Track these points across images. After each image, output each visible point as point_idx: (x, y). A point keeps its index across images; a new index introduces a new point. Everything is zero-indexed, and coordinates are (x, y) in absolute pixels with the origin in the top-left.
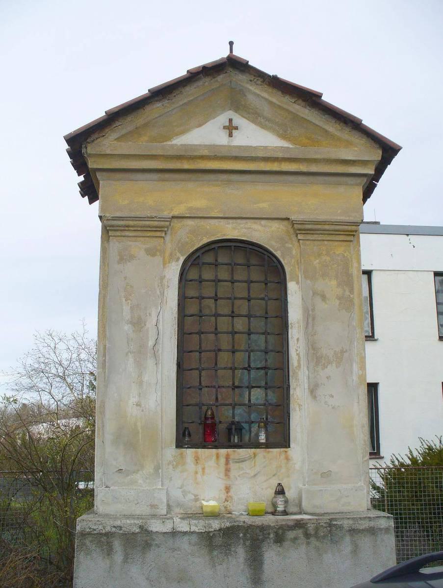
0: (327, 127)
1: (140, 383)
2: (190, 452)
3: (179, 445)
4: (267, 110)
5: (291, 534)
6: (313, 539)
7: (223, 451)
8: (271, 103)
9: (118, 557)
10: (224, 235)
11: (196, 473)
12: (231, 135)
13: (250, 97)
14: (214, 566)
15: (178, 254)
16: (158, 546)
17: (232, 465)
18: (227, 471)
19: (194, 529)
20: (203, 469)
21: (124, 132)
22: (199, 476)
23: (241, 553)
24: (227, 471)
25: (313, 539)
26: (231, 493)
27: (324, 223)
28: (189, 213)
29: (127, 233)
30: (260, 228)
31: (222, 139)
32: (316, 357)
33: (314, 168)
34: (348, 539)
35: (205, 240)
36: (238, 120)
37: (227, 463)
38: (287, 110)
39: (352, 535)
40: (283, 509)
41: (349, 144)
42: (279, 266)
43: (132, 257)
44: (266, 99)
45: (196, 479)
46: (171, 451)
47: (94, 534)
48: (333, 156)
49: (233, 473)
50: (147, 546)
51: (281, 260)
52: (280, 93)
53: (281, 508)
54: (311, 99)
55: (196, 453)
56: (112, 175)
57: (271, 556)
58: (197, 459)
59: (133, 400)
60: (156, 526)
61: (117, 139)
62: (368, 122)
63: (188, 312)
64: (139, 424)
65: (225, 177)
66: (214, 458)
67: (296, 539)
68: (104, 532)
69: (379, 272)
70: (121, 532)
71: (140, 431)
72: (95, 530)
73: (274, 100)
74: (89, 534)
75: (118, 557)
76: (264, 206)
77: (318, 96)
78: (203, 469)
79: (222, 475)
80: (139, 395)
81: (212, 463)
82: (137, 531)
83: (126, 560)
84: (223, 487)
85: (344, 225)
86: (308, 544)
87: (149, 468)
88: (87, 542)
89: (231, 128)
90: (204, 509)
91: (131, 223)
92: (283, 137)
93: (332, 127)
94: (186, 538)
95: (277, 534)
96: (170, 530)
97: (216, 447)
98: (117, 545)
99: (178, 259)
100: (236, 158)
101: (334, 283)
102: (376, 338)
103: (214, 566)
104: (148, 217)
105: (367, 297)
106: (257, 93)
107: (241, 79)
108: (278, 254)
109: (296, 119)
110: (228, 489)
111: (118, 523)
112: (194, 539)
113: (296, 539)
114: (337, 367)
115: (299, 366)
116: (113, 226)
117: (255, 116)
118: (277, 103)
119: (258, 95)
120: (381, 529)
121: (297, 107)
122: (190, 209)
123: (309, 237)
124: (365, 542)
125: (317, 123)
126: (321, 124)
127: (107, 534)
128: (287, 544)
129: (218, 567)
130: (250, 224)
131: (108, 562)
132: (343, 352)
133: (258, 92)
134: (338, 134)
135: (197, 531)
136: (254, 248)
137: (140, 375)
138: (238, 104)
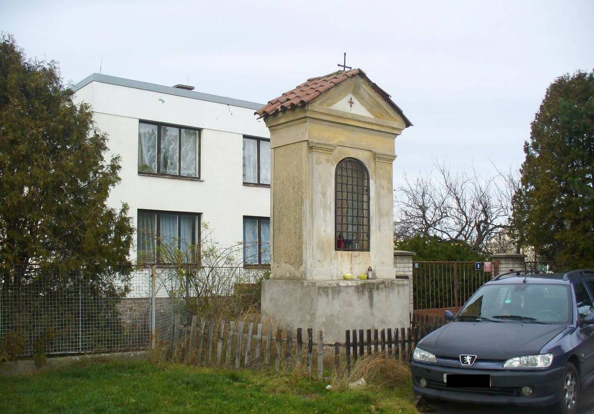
0: (390, 112)
1: (325, 221)
2: (339, 252)
4: (366, 97)
5: (381, 286)
6: (387, 288)
7: (350, 252)
8: (370, 95)
9: (330, 297)
12: (351, 106)
13: (362, 91)
14: (359, 300)
15: (335, 163)
16: (342, 292)
17: (353, 259)
18: (351, 261)
19: (353, 284)
20: (344, 260)
22: (342, 263)
23: (367, 294)
24: (351, 261)
25: (387, 288)
29: (320, 151)
30: (361, 153)
32: (381, 214)
33: (383, 129)
34: (396, 288)
36: (354, 100)
37: (351, 258)
38: (376, 100)
39: (397, 287)
40: (308, 278)
41: (395, 120)
43: (321, 163)
44: (368, 93)
46: (333, 251)
48: (390, 125)
49: (353, 262)
50: (339, 292)
53: (370, 277)
54: (385, 96)
55: (341, 253)
56: (316, 121)
57: (375, 294)
58: (342, 256)
59: (323, 229)
60: (343, 284)
61: (319, 104)
62: (404, 113)
63: (338, 190)
64: (325, 240)
65: (352, 128)
67: (382, 288)
69: (207, 130)
73: (371, 94)
74: (321, 287)
75: (330, 297)
79: (350, 263)
81: (346, 257)
83: (333, 298)
84: (350, 268)
86: (386, 290)
87: (329, 260)
88: (320, 291)
89: (351, 103)
91: (323, 146)
92: (369, 110)
93: (390, 111)
94: (351, 288)
95: (377, 286)
97: (348, 251)
98: (330, 291)
100: (359, 121)
102: (201, 179)
103: (359, 300)
106: (365, 89)
107: (361, 81)
108: (367, 166)
109: (378, 104)
110: (351, 269)
111: (330, 283)
112: (353, 288)
113: (382, 288)
114: (387, 218)
115: (373, 217)
116: (315, 147)
117: (361, 99)
118: (373, 96)
119: (366, 90)
120: (405, 284)
121: (380, 99)
122: (340, 142)
123: (380, 161)
124: (401, 289)
126: (386, 109)
127: (327, 287)
128: (380, 290)
129: (360, 300)
131: (327, 299)
132: (388, 212)
133: (366, 88)
134: (393, 115)
137: (325, 218)
138: (355, 92)
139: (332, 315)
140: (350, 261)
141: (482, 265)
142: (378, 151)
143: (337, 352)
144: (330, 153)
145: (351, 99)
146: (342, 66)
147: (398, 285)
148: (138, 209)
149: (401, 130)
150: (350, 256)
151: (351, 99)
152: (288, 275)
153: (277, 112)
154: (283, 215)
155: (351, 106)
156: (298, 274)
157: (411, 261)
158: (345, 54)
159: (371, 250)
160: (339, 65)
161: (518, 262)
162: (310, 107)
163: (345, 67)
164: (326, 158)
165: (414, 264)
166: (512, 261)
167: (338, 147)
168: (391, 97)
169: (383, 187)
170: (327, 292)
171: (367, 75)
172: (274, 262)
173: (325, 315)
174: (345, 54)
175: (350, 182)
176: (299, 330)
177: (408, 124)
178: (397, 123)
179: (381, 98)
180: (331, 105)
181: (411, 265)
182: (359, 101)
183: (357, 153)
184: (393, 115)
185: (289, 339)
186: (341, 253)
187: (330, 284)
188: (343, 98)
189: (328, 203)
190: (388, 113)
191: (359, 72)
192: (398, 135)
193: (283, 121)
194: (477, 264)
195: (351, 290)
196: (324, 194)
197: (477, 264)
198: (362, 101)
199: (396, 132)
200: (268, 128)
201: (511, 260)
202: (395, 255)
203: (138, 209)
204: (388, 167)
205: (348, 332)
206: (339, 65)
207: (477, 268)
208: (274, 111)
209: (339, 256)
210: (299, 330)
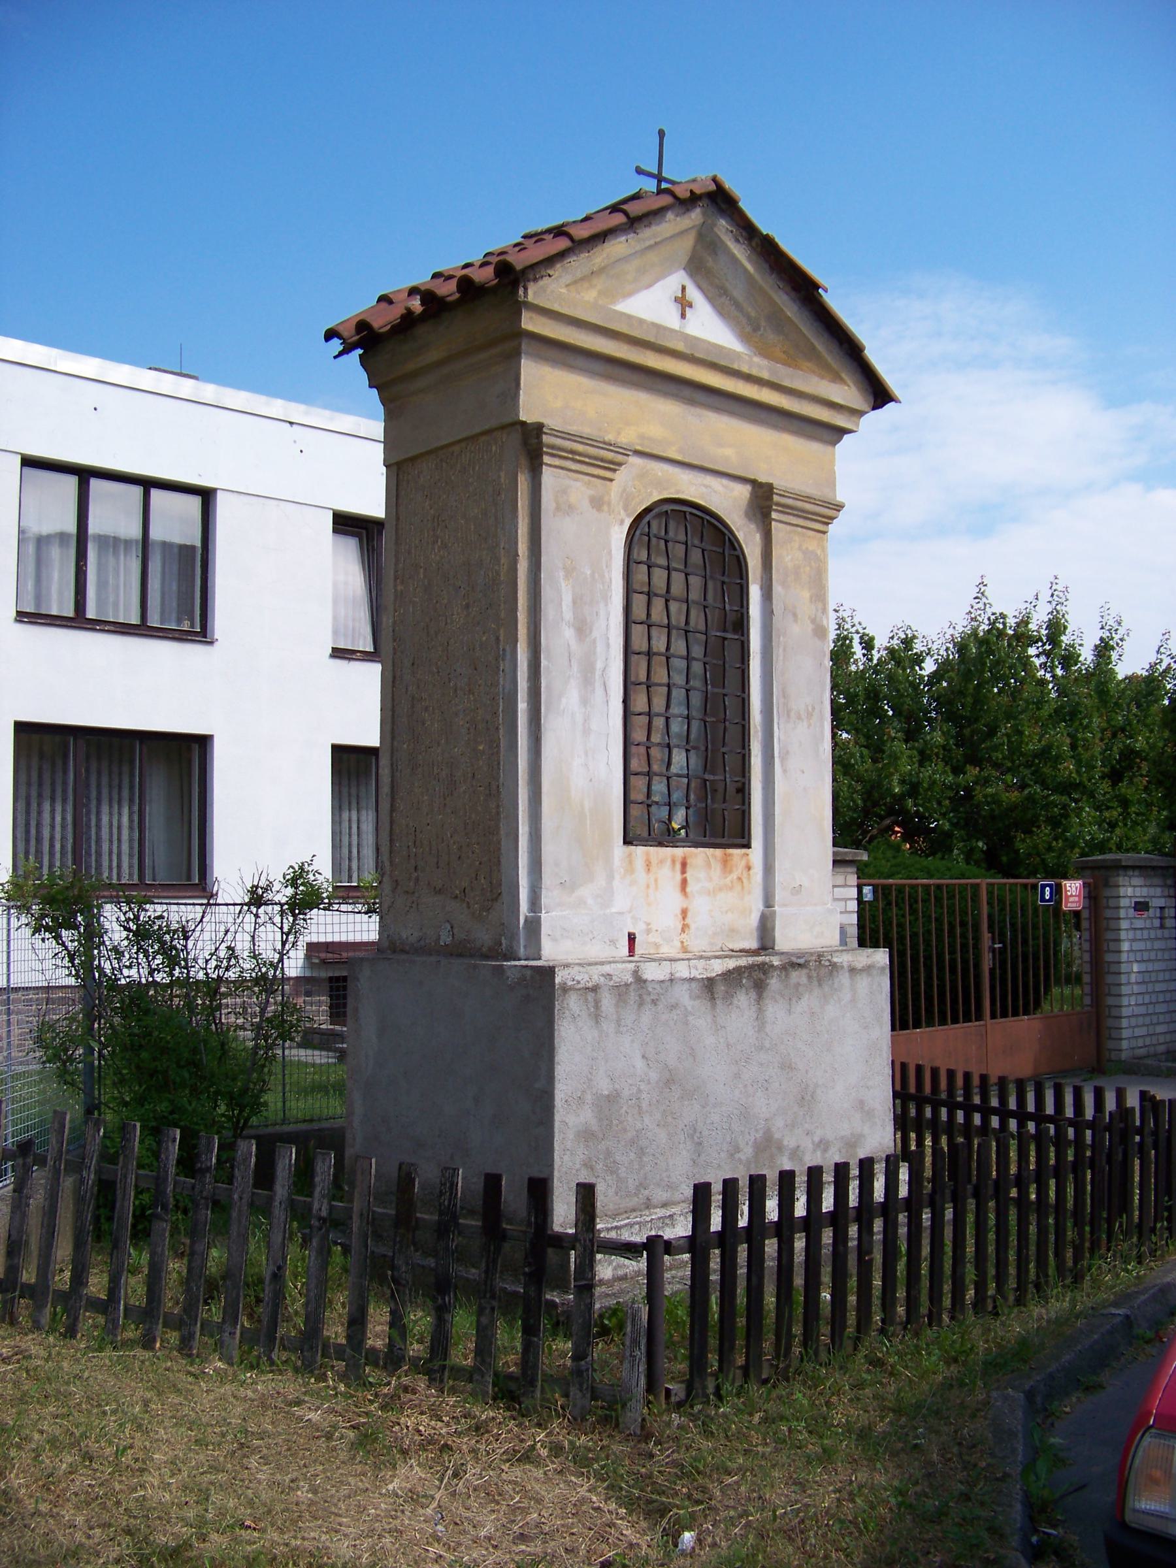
2: (640, 851)
3: (627, 842)
4: (738, 293)
10: (678, 492)
11: (648, 887)
12: (683, 316)
19: (695, 974)
21: (579, 275)
26: (688, 921)
27: (808, 499)
28: (641, 445)
31: (669, 317)
35: (656, 497)
36: (693, 294)
39: (851, 978)
41: (837, 378)
42: (741, 557)
43: (570, 509)
45: (647, 896)
46: (618, 849)
47: (579, 989)
51: (744, 546)
52: (766, 266)
55: (648, 854)
58: (648, 865)
65: (687, 392)
66: (669, 862)
68: (590, 985)
70: (612, 983)
71: (588, 814)
72: (579, 982)
75: (608, 1026)
76: (727, 456)
77: (816, 286)
78: (656, 880)
79: (678, 889)
80: (586, 754)
82: (631, 980)
85: (829, 508)
89: (683, 304)
90: (1087, 905)
91: (580, 448)
92: (744, 337)
96: (668, 977)
98: (607, 1002)
99: (622, 522)
101: (806, 594)
104: (604, 443)
105: (193, 548)
110: (684, 913)
111: (607, 969)
122: (642, 437)
125: (805, 332)
127: (595, 989)
130: (710, 480)
135: (699, 977)
136: (713, 521)
137: (586, 720)
139: (612, 1098)
140: (679, 877)
141: (1058, 890)
142: (780, 481)
143: (653, 1274)
144: (608, 474)
145: (684, 288)
146: (650, 175)
147: (853, 970)
148: (22, 728)
149: (861, 413)
150: (678, 866)
151: (684, 288)
152: (445, 938)
153: (408, 321)
154: (426, 709)
155: (683, 316)
156: (483, 937)
157: (853, 879)
158: (661, 134)
159: (753, 845)
160: (639, 171)
161: (1156, 881)
162: (534, 293)
163: (660, 179)
164: (591, 492)
165: (860, 888)
166: (1140, 876)
167: (634, 460)
168: (826, 291)
169: (795, 615)
170: (597, 1004)
171: (741, 204)
172: (394, 890)
173: (589, 1098)
174: (661, 134)
175: (677, 588)
176: (493, 1182)
177: (880, 395)
178: (847, 393)
179: (793, 294)
180: (614, 303)
181: (854, 892)
182: (710, 300)
183: (706, 486)
184: (829, 359)
185: (446, 1225)
186: (648, 854)
187: (609, 976)
188: (657, 280)
189: (599, 665)
190: (814, 348)
191: (713, 187)
192: (849, 431)
193: (433, 355)
194: (1044, 887)
195: (682, 995)
196: (582, 629)
197: (1044, 887)
198: (723, 299)
199: (840, 421)
200: (375, 390)
201: (1137, 873)
202: (836, 863)
203: (22, 728)
204: (812, 545)
205: (701, 1193)
206: (639, 171)
207: (1043, 900)
208: (389, 327)
209: (639, 863)
210: (493, 1182)
